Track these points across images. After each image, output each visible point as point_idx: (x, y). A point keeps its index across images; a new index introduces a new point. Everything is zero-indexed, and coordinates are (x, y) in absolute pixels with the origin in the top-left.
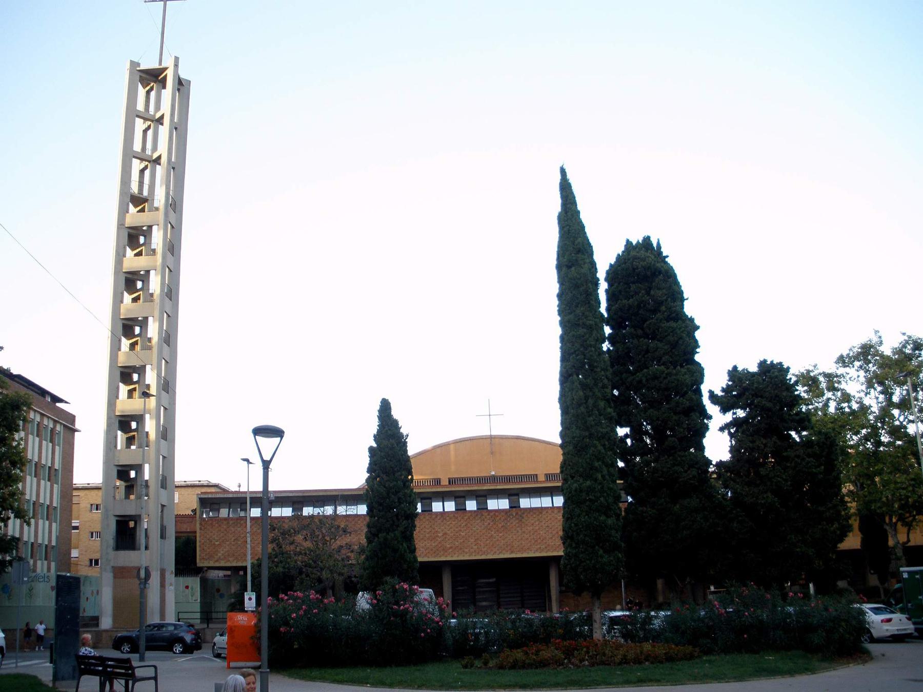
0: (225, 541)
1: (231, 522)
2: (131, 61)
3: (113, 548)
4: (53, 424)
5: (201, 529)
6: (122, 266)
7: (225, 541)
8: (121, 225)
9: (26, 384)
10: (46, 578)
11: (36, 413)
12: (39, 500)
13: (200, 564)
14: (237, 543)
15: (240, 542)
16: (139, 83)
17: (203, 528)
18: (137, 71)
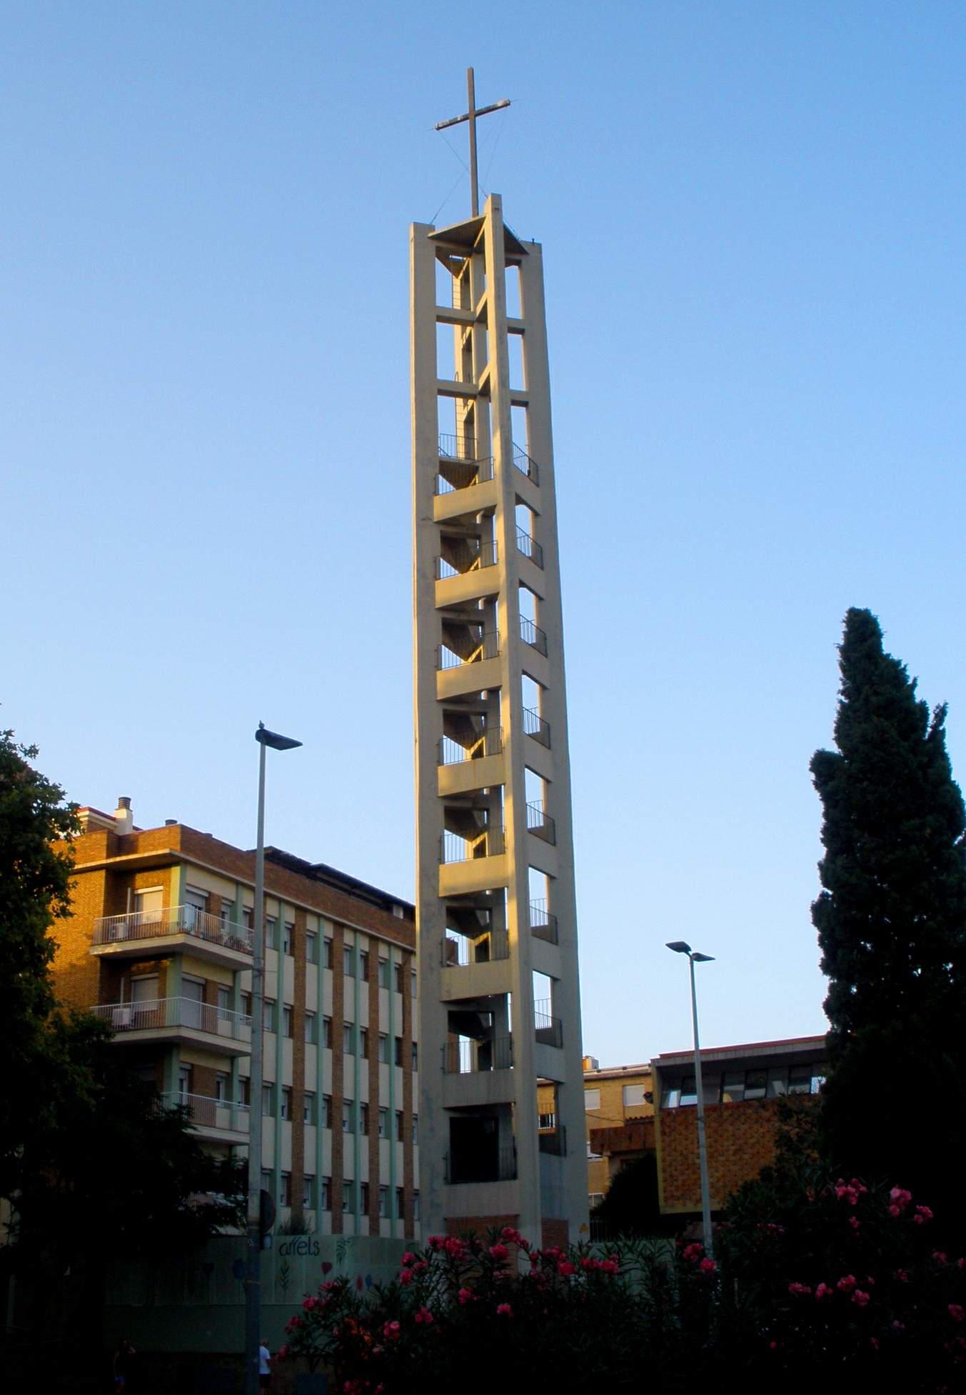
0: (716, 1154)
1: (726, 1114)
2: (415, 224)
3: (446, 1179)
4: (403, 958)
5: (663, 1133)
6: (434, 598)
7: (716, 1154)
8: (423, 520)
9: (346, 886)
10: (312, 1245)
11: (392, 948)
12: (302, 1084)
13: (666, 1208)
14: (741, 1159)
15: (746, 1156)
16: (436, 259)
17: (667, 1130)
18: (429, 240)
